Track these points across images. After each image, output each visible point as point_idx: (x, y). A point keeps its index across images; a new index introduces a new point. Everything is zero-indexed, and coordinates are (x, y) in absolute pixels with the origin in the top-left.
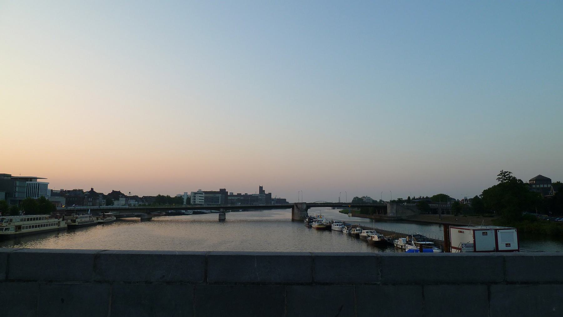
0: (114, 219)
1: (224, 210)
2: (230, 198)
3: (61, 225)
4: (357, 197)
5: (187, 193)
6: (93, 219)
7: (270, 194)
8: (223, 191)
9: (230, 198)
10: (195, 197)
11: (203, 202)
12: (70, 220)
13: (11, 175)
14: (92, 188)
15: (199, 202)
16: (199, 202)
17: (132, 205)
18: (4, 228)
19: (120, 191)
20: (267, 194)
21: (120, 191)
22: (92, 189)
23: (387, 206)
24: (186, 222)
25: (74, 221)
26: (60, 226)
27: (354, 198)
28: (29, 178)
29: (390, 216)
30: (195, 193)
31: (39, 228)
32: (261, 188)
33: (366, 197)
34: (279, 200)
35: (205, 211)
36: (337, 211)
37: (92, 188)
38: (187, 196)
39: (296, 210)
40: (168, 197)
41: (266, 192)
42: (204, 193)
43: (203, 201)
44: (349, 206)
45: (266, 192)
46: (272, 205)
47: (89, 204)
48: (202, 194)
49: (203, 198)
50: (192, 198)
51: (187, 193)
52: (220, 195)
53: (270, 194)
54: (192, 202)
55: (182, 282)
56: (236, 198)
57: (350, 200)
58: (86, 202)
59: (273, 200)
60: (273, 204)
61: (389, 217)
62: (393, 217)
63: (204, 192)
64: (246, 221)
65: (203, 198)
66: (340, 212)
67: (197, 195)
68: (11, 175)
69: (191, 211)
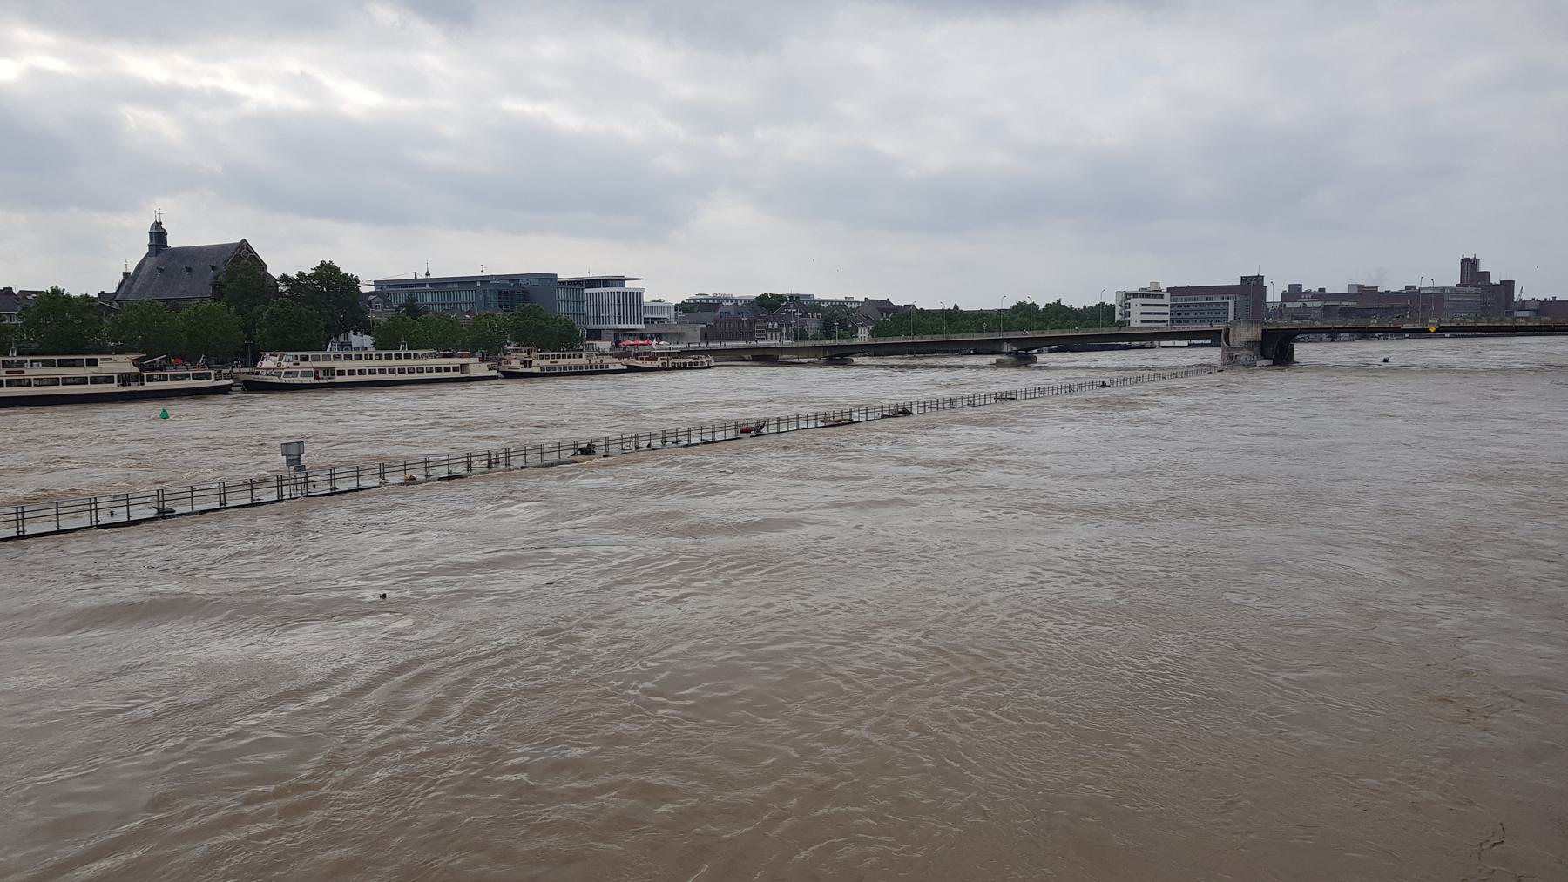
5: (1301, 285)
6: (602, 361)
7: (1508, 286)
12: (519, 362)
14: (1464, 261)
15: (1143, 322)
16: (1143, 322)
18: (283, 372)
20: (1496, 285)
24: (893, 367)
28: (600, 280)
30: (1127, 296)
31: (1125, 376)
32: (1469, 265)
37: (1464, 261)
44: (1428, 330)
46: (1521, 322)
49: (1167, 310)
50: (1118, 310)
51: (1301, 285)
53: (1508, 286)
55: (790, 476)
58: (763, 331)
59: (1523, 305)
60: (1522, 317)
64: (1446, 369)
65: (1167, 310)
67: (1133, 301)
68: (126, 274)
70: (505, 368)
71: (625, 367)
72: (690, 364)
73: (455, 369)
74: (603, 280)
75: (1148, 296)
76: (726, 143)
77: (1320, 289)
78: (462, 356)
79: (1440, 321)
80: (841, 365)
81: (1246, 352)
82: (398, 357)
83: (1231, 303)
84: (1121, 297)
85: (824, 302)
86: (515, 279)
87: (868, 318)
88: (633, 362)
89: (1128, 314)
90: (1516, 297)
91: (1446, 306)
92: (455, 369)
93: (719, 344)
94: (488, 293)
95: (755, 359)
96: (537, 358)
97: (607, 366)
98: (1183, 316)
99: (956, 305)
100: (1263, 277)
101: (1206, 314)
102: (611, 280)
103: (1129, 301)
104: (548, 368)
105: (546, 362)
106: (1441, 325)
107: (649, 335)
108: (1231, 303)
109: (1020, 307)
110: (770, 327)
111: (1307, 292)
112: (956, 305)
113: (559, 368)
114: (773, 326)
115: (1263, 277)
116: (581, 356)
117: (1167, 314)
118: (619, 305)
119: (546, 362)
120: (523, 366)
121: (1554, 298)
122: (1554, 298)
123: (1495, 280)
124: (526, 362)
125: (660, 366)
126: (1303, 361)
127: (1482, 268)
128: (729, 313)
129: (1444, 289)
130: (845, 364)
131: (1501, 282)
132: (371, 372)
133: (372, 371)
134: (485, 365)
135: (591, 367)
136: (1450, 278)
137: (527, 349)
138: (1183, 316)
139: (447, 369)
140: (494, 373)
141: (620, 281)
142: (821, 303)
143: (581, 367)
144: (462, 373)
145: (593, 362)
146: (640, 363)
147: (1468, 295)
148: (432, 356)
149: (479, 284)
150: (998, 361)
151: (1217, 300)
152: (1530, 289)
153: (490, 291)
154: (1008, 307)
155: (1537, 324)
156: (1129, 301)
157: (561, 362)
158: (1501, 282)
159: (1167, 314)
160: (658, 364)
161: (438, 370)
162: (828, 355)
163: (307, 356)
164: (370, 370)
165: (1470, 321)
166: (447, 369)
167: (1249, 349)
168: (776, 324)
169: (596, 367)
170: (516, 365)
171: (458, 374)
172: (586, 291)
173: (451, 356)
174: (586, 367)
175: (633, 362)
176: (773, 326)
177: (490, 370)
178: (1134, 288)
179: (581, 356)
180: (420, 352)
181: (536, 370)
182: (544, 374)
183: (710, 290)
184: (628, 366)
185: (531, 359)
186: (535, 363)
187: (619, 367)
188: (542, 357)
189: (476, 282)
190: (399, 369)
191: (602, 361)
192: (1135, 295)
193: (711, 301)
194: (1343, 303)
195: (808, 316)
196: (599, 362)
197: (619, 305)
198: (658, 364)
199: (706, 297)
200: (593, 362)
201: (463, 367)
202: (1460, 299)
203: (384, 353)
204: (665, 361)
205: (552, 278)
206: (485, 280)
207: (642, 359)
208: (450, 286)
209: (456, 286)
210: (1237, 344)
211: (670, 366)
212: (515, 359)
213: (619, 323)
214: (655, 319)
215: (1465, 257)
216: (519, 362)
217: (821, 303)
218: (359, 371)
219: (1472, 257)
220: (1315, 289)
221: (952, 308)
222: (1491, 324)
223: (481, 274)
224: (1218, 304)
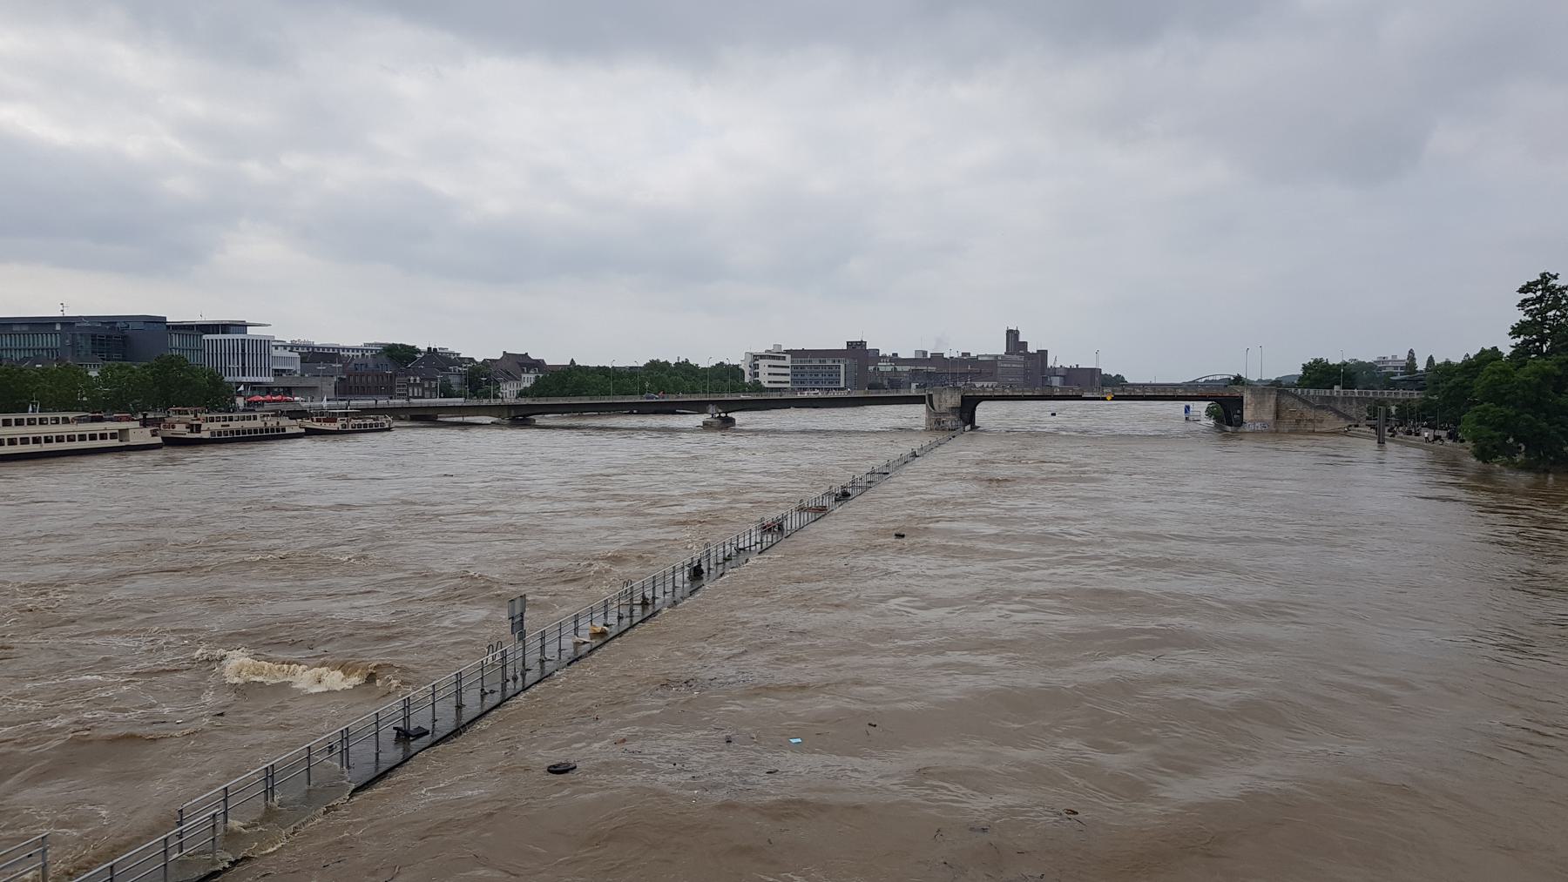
3: (131, 441)
6: (278, 423)
7: (1043, 354)
8: (857, 349)
10: (756, 367)
12: (184, 426)
13: (165, 318)
14: (1009, 332)
16: (769, 382)
19: (527, 354)
20: (1033, 354)
21: (527, 354)
22: (504, 352)
23: (1242, 397)
25: (198, 429)
26: (128, 441)
28: (218, 325)
30: (756, 357)
32: (1012, 335)
33: (1390, 358)
35: (385, 420)
37: (1009, 332)
40: (686, 369)
41: (1032, 349)
42: (788, 357)
43: (788, 379)
47: (413, 391)
48: (784, 358)
49: (788, 371)
53: (1043, 354)
56: (906, 368)
59: (1054, 371)
63: (787, 352)
67: (761, 362)
68: (165, 318)
70: (168, 433)
71: (303, 430)
72: (371, 425)
73: (113, 436)
74: (222, 325)
75: (773, 357)
76: (254, 169)
77: (893, 354)
78: (119, 420)
79: (1113, 391)
80: (523, 425)
81: (951, 417)
82: (31, 422)
83: (842, 366)
84: (750, 359)
85: (343, 349)
86: (111, 322)
87: (508, 373)
88: (309, 424)
89: (757, 375)
90: (1049, 366)
91: (999, 370)
92: (113, 436)
93: (385, 401)
94: (79, 337)
95: (413, 419)
96: (206, 420)
97: (284, 430)
98: (799, 377)
99: (572, 360)
101: (820, 376)
102: (236, 325)
103: (757, 362)
104: (220, 433)
105: (216, 426)
106: (1116, 394)
107: (276, 390)
108: (842, 366)
109: (654, 365)
110: (412, 382)
111: (884, 357)
112: (572, 360)
113: (232, 432)
114: (415, 380)
116: (255, 418)
117: (788, 375)
118: (243, 355)
119: (216, 426)
120: (189, 430)
121: (1077, 366)
122: (1077, 366)
123: (1032, 349)
124: (192, 425)
125: (340, 429)
126: (985, 427)
127: (1021, 339)
128: (367, 366)
129: (997, 356)
130: (525, 425)
131: (1038, 351)
132: (48, 440)
133: (71, 438)
134: (148, 431)
135: (267, 431)
136: (996, 346)
137: (193, 409)
138: (799, 377)
139: (103, 437)
140: (158, 440)
141: (242, 327)
142: (341, 351)
143: (256, 431)
144: (121, 441)
145: (269, 425)
146: (317, 426)
147: (1012, 362)
148: (79, 420)
149: (58, 327)
150: (705, 424)
151: (829, 363)
152: (1059, 358)
153: (81, 335)
154: (641, 365)
155: (1195, 394)
156: (757, 362)
157: (234, 425)
158: (1038, 351)
159: (788, 375)
160: (337, 426)
161: (82, 438)
162: (513, 415)
163: (23, 419)
164: (46, 438)
165: (1138, 390)
166: (103, 437)
167: (954, 414)
168: (418, 378)
169: (273, 430)
170: (181, 430)
171: (116, 443)
172: (205, 337)
173: (100, 420)
174: (261, 431)
175: (309, 424)
176: (415, 380)
177: (153, 436)
178: (761, 350)
179: (255, 418)
180: (71, 416)
181: (205, 435)
182: (216, 441)
183: (403, 343)
184: (306, 429)
185: (199, 422)
186: (204, 426)
187: (297, 430)
188: (212, 420)
189: (55, 324)
190: (57, 437)
191: (278, 423)
192: (762, 357)
193: (316, 350)
194: (930, 368)
195: (450, 371)
196: (275, 424)
197: (243, 355)
198: (337, 426)
199: (283, 344)
200: (269, 425)
201: (123, 433)
202: (1009, 366)
203: (49, 416)
204: (344, 422)
205: (160, 321)
206: (68, 323)
207: (318, 421)
208: (16, 328)
209: (25, 328)
210: (943, 409)
211: (350, 429)
212: (179, 422)
213: (244, 375)
214: (284, 371)
215: (1010, 328)
216: (184, 426)
217: (341, 351)
218: (34, 439)
219: (1015, 329)
220: (889, 354)
221: (569, 364)
222: (1157, 394)
223: (60, 314)
224: (830, 367)
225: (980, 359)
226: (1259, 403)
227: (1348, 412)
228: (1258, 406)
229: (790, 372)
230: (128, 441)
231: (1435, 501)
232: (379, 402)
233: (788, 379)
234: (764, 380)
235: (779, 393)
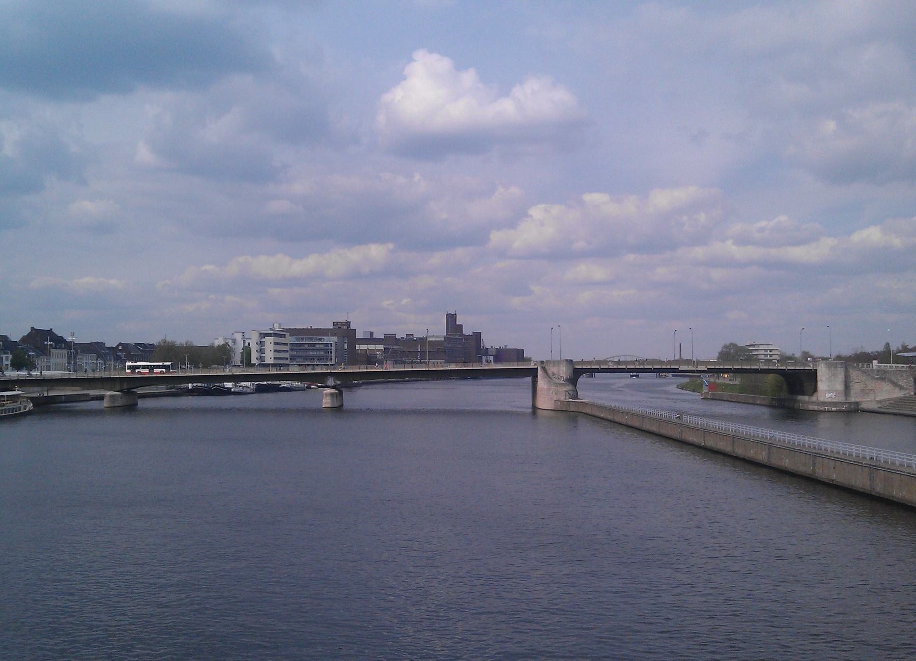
0: (27, 409)
1: (339, 382)
2: (363, 347)
3: (266, 361)
4: (735, 345)
7: (477, 336)
9: (363, 347)
11: (287, 359)
17: (898, 463)
27: (725, 347)
29: (826, 400)
34: (500, 355)
36: (671, 384)
38: (244, 342)
39: (542, 383)
41: (467, 331)
45: (467, 331)
49: (287, 348)
52: (333, 340)
53: (477, 336)
54: (254, 361)
57: (709, 354)
61: (824, 403)
62: (835, 404)
66: (682, 387)
67: (269, 340)
69: (248, 384)
100: (350, 322)
115: (350, 322)
121: (500, 347)
131: (474, 333)
136: (438, 330)
156: (264, 340)
225: (428, 339)
226: (833, 375)
227: (900, 383)
228: (833, 378)
229: (289, 350)
230: (265, 361)
231: (301, 392)
232: (38, 373)
233: (287, 355)
234: (269, 358)
235: (267, 369)
